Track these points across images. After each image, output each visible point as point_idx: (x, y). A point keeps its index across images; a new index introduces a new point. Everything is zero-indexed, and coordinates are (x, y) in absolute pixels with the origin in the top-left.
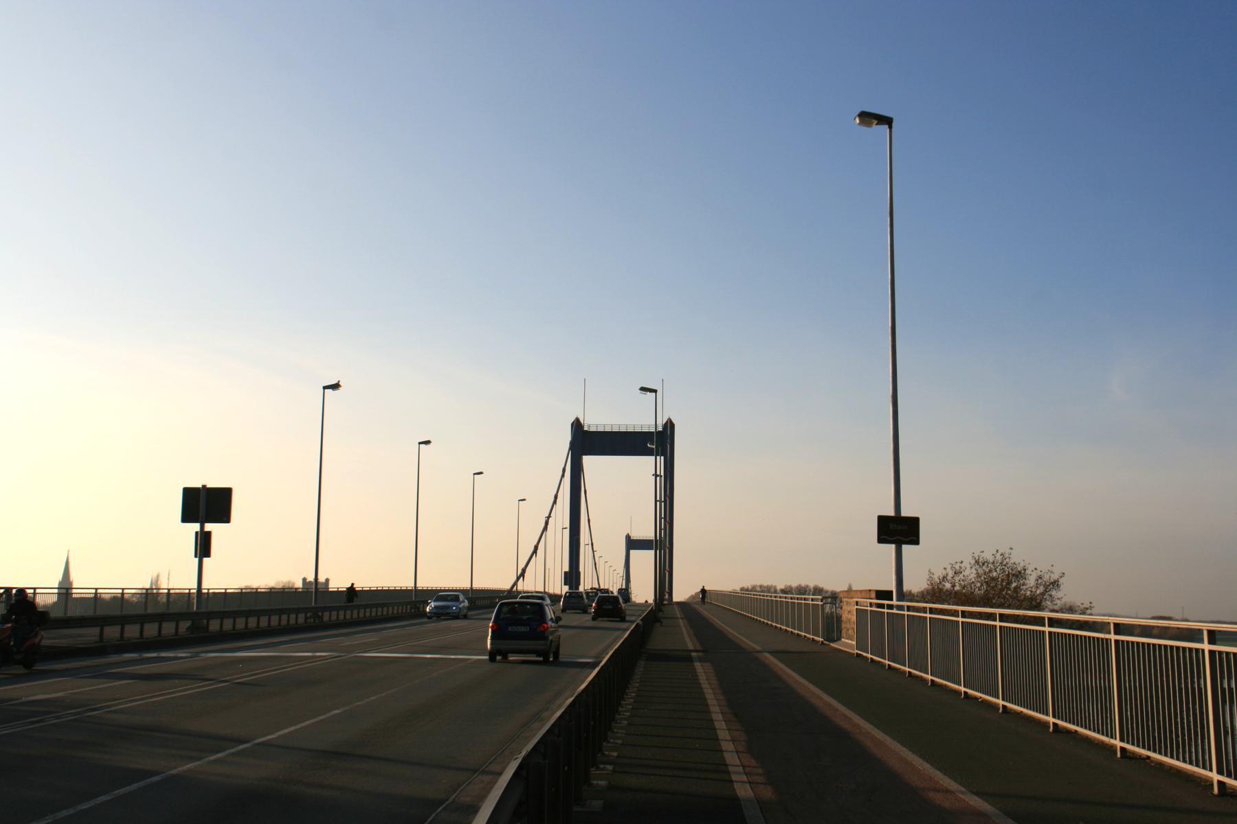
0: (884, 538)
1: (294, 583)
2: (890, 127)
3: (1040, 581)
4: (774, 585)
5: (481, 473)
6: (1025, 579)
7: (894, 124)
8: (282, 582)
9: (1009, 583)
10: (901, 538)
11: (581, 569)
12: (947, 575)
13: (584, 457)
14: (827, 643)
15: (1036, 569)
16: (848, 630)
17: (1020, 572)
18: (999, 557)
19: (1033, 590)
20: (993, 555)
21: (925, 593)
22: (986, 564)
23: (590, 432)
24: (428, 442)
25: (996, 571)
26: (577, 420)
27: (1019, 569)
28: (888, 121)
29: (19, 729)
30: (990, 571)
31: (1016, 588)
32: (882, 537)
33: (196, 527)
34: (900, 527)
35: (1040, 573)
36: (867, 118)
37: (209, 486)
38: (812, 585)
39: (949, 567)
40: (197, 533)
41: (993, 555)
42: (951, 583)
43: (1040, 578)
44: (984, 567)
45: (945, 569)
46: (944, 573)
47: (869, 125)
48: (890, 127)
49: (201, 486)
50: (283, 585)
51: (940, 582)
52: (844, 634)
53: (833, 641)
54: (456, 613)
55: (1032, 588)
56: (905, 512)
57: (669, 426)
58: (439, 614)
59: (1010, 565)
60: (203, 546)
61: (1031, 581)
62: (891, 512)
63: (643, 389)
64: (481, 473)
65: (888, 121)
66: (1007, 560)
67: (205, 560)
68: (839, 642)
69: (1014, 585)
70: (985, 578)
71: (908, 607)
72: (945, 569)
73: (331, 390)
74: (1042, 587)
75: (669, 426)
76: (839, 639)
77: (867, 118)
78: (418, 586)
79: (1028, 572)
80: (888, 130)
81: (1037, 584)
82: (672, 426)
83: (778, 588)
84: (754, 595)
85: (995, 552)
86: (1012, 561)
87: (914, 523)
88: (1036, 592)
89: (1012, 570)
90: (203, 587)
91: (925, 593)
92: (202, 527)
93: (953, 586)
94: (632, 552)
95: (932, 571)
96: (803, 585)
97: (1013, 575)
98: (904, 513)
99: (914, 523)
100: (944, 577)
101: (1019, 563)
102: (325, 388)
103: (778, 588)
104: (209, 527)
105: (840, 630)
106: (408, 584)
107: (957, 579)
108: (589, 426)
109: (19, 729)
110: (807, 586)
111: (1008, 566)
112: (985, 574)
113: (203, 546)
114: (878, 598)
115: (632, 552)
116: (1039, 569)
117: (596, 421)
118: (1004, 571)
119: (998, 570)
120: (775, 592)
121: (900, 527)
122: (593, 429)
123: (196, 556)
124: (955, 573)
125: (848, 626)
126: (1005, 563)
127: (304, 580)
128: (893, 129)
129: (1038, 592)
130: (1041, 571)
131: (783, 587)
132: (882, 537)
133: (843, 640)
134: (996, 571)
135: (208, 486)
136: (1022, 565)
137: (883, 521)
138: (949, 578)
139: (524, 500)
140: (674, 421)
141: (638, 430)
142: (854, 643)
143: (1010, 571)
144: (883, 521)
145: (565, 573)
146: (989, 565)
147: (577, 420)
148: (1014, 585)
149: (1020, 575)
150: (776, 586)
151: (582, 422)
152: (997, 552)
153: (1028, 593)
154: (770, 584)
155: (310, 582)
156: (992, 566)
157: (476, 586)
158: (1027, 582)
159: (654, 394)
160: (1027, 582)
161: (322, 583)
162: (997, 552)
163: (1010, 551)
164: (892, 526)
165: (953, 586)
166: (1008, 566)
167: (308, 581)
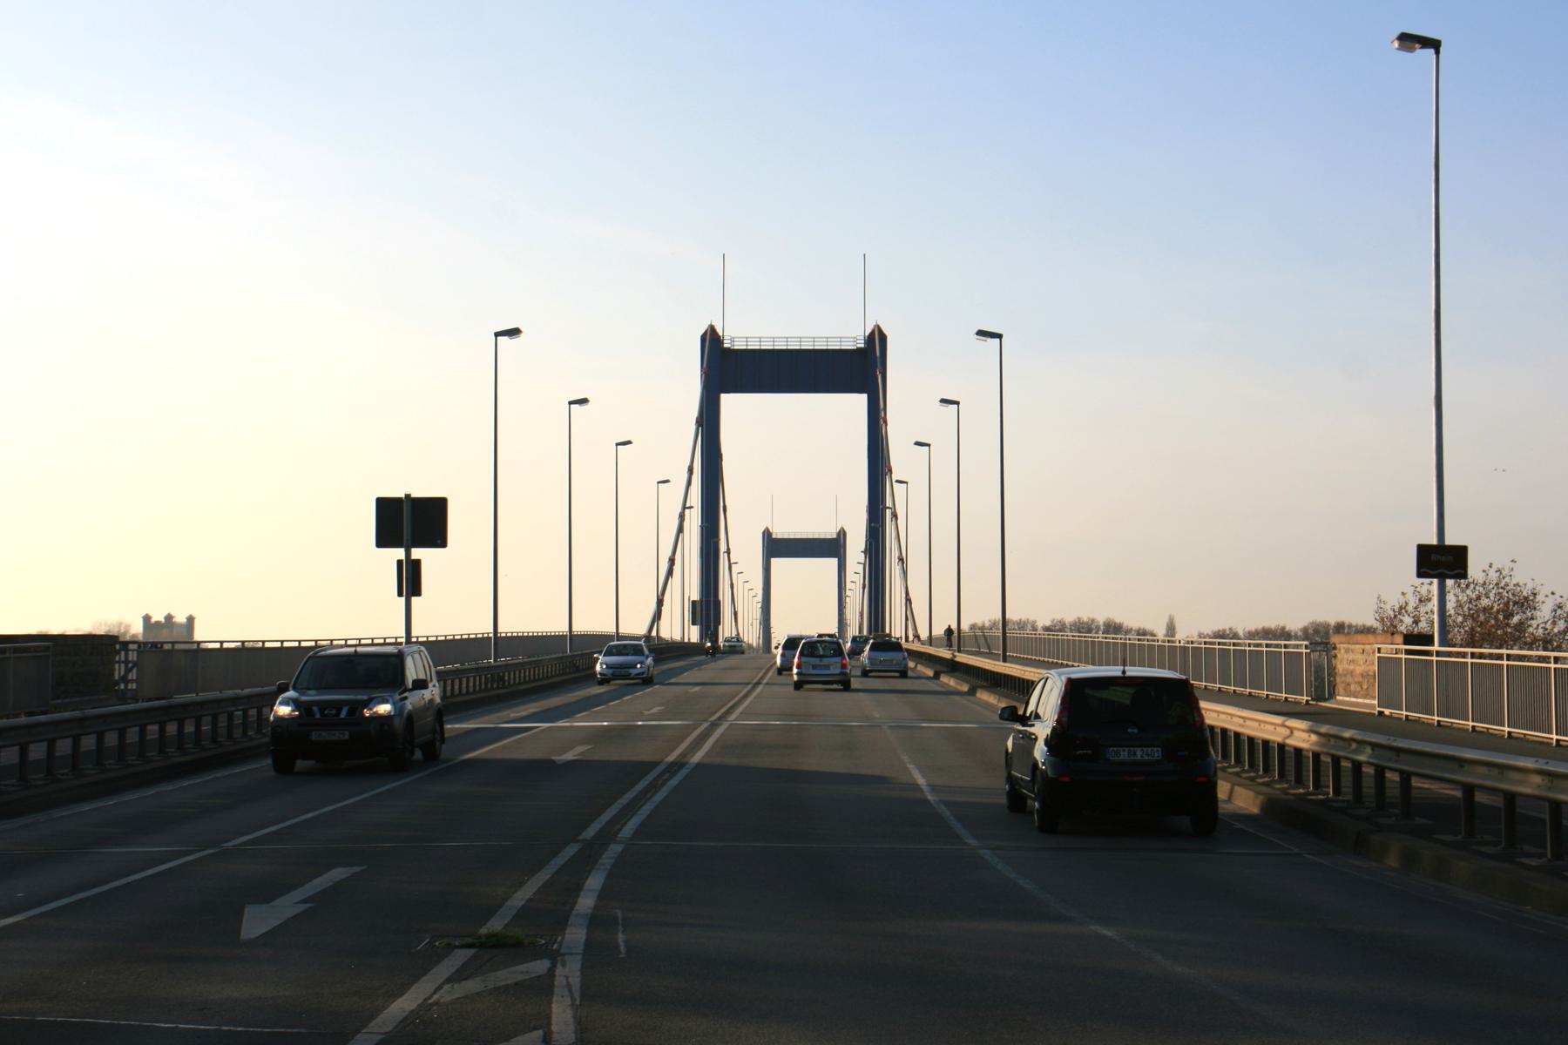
0: (1424, 572)
1: (128, 626)
2: (1437, 53)
3: (1559, 612)
4: (1032, 618)
5: (629, 442)
6: (1535, 609)
7: (1441, 49)
8: (106, 624)
9: (1509, 615)
10: (1428, 570)
11: (721, 598)
12: (1407, 603)
13: (723, 396)
14: (1314, 703)
15: (1553, 593)
16: (1349, 685)
17: (1526, 599)
18: (1493, 576)
19: (1549, 626)
20: (1484, 571)
21: (1311, 631)
22: (1472, 586)
23: (734, 350)
24: (583, 401)
25: (1488, 597)
26: (712, 329)
27: (1525, 594)
28: (1434, 45)
29: (1347, 699)
30: (1479, 598)
31: (1521, 623)
32: (1422, 570)
33: (399, 553)
34: (1444, 558)
35: (1559, 600)
36: (1409, 41)
37: (414, 495)
38: (1101, 619)
39: (1410, 591)
40: (400, 563)
41: (1484, 571)
42: (1413, 617)
43: (1560, 607)
44: (1468, 592)
45: (1403, 594)
46: (1402, 601)
47: (1411, 50)
48: (1437, 53)
49: (403, 496)
50: (107, 629)
51: (1395, 616)
52: (1340, 688)
53: (1325, 700)
54: (643, 673)
55: (1546, 623)
56: (1450, 540)
57: (877, 340)
58: (617, 673)
59: (1511, 587)
60: (410, 581)
61: (1544, 613)
62: (1433, 540)
63: (981, 333)
64: (629, 442)
65: (1434, 45)
66: (1507, 579)
67: (414, 600)
68: (1334, 700)
69: (1516, 619)
70: (1470, 609)
71: (1508, 656)
72: (1403, 594)
73: (506, 338)
74: (1562, 621)
75: (877, 340)
76: (1332, 695)
77: (1409, 41)
78: (500, 630)
79: (1540, 598)
80: (1434, 56)
81: (1554, 617)
82: (883, 338)
83: (1040, 624)
84: (1053, 635)
85: (1487, 568)
86: (1514, 582)
87: (1460, 553)
88: (1552, 629)
89: (1513, 595)
90: (413, 635)
91: (1311, 631)
92: (408, 554)
93: (1416, 622)
94: (774, 561)
95: (1383, 598)
96: (1085, 620)
97: (1515, 603)
98: (1449, 541)
99: (1460, 553)
100: (1401, 608)
101: (1525, 585)
102: (497, 334)
103: (1040, 624)
104: (417, 553)
105: (1333, 687)
106: (561, 627)
107: (1422, 610)
108: (732, 340)
109: (1347, 699)
110: (1093, 621)
111: (1508, 588)
112: (1470, 602)
113: (410, 581)
114: (1405, 643)
115: (775, 562)
116: (1558, 594)
117: (741, 334)
118: (1501, 597)
119: (1492, 595)
120: (1236, 636)
121: (1444, 558)
122: (739, 346)
123: (400, 594)
124: (1420, 601)
125: (1349, 679)
126: (1502, 584)
127: (147, 619)
128: (1441, 55)
129: (1556, 630)
130: (1561, 597)
131: (1048, 624)
132: (1422, 570)
133: (1338, 698)
134: (1488, 597)
135: (413, 496)
136: (1530, 586)
137: (1424, 552)
138: (1410, 608)
139: (667, 481)
140: (885, 331)
141: (834, 346)
142: (1376, 702)
143: (1511, 597)
144: (1424, 552)
145: (694, 603)
146: (1477, 588)
147: (712, 329)
148: (1516, 619)
149: (1526, 603)
150: (1035, 622)
151: (721, 334)
152: (1490, 567)
153: (1540, 631)
154: (1024, 618)
155: (158, 623)
156: (1481, 589)
157: (508, 627)
158: (1538, 614)
159: (998, 340)
160: (1538, 614)
161: (180, 625)
162: (1490, 567)
163: (1512, 565)
164: (1434, 557)
165: (1416, 622)
166: (1508, 588)
167: (154, 620)
